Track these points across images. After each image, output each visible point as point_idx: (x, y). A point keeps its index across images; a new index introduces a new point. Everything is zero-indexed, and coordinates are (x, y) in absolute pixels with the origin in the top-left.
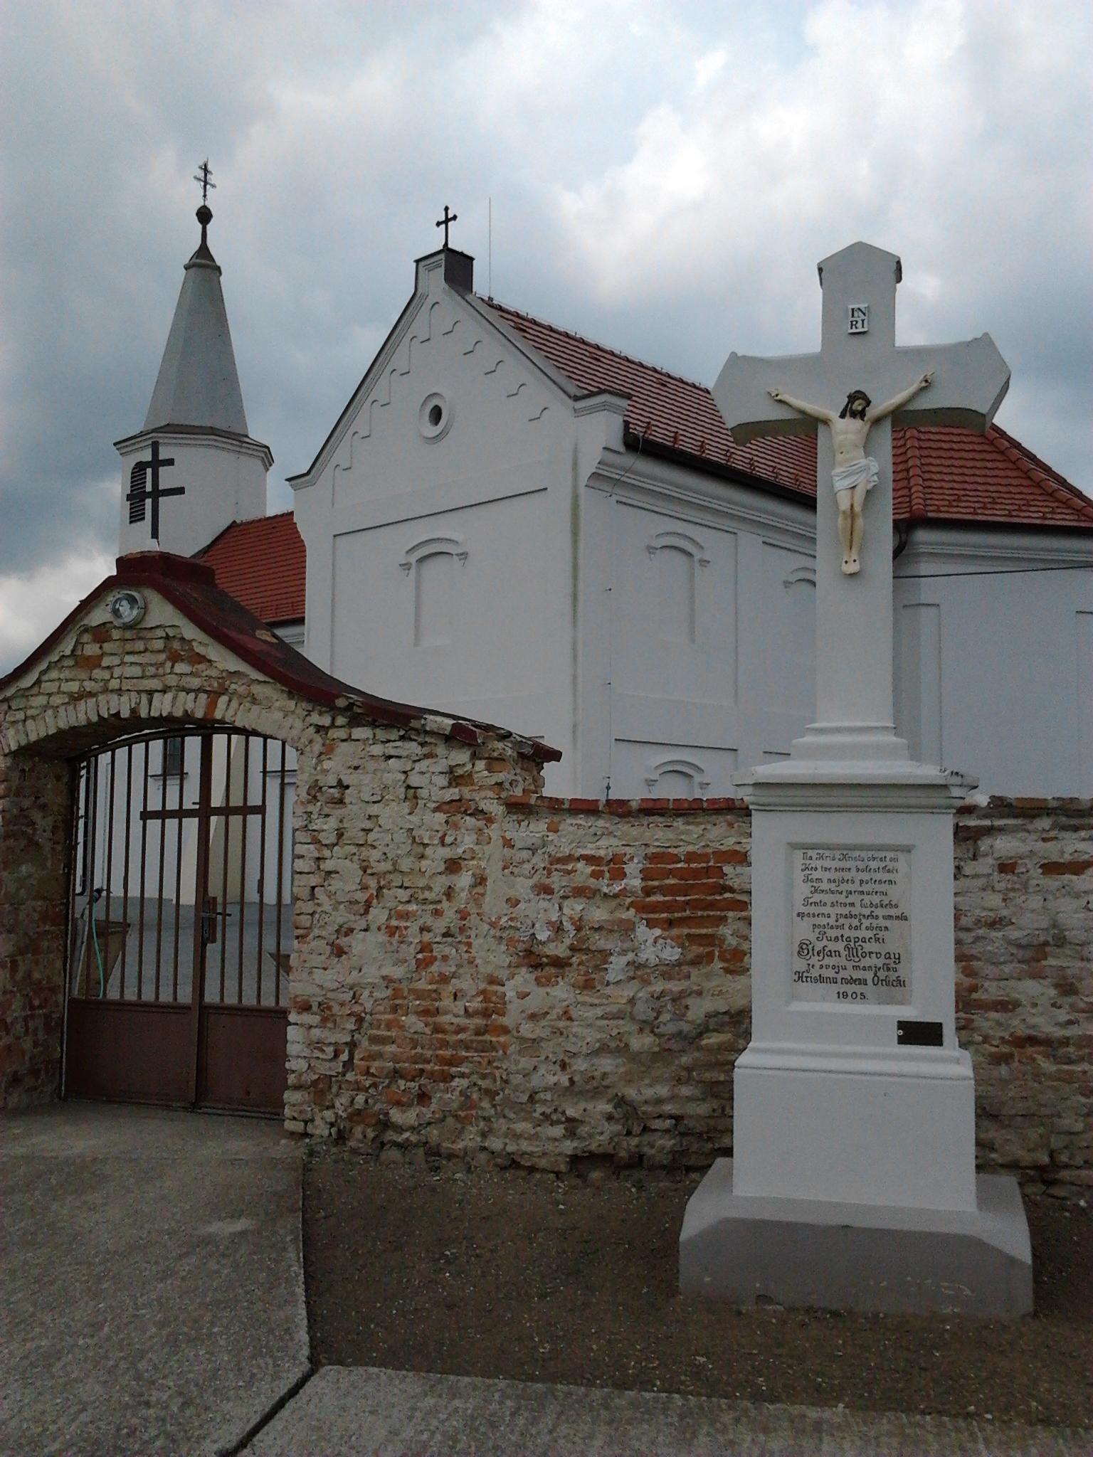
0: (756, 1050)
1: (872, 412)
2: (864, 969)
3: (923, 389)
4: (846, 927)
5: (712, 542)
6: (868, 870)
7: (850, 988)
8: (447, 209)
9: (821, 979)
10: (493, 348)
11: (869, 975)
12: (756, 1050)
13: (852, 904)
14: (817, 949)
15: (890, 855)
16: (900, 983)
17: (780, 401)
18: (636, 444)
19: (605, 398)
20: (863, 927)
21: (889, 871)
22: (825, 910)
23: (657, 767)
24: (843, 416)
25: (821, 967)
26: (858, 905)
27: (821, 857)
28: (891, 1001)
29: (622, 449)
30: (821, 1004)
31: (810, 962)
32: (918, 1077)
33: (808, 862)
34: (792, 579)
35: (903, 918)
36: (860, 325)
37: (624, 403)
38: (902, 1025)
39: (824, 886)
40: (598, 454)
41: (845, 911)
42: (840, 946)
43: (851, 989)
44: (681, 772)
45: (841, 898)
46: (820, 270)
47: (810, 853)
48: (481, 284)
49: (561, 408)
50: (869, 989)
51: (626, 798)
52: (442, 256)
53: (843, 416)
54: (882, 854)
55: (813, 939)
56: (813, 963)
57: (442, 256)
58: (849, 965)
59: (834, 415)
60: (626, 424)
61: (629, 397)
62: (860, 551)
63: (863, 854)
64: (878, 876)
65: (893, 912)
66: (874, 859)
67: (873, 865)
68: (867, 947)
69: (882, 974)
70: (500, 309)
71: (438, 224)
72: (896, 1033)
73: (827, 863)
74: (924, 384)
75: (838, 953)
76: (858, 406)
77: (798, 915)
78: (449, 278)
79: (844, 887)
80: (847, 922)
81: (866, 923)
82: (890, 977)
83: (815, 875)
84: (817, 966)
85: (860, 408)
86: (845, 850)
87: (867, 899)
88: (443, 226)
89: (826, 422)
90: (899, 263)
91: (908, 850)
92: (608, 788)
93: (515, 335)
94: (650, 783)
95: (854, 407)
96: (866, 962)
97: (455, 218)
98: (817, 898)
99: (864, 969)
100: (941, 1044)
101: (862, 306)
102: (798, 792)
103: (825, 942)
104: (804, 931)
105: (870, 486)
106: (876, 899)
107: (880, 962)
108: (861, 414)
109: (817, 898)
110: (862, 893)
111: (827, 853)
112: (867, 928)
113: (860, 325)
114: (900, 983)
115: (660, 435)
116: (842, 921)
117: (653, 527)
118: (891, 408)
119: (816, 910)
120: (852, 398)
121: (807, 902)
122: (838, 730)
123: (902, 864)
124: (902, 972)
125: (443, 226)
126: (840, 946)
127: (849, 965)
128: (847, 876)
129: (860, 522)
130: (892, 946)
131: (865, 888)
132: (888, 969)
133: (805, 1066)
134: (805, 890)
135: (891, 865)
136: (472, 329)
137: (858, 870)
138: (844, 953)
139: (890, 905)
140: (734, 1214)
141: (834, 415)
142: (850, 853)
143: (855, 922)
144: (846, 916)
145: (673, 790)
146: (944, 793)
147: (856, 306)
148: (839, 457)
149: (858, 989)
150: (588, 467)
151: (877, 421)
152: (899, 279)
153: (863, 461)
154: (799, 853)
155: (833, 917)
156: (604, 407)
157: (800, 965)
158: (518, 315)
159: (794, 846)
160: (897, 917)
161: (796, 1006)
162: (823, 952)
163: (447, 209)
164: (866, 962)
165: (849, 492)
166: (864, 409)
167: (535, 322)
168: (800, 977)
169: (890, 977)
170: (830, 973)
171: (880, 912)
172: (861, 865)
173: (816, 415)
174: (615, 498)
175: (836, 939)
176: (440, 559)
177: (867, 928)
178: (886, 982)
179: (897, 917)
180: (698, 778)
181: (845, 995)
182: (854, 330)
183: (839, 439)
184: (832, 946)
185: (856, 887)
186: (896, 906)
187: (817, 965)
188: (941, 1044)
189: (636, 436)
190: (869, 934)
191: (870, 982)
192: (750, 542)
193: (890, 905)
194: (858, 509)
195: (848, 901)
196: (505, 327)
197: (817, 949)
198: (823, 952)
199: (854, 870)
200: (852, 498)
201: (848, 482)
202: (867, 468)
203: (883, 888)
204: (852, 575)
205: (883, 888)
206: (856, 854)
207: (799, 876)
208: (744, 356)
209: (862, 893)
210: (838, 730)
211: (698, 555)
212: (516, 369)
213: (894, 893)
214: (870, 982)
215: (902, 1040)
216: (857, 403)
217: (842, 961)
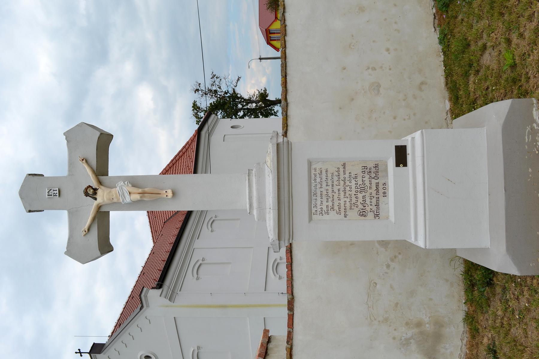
0: (416, 239)
1: (95, 184)
2: (370, 184)
3: (87, 161)
4: (350, 193)
5: (197, 257)
6: (321, 183)
7: (381, 191)
8: (76, 353)
9: (377, 205)
10: (125, 337)
11: (374, 182)
12: (416, 239)
13: (339, 190)
14: (362, 207)
15: (313, 172)
16: (376, 166)
17: (89, 230)
18: (160, 286)
19: (142, 295)
20: (350, 184)
21: (321, 172)
22: (342, 205)
23: (275, 275)
24: (96, 199)
25: (371, 205)
26: (339, 187)
27: (316, 206)
28: (386, 170)
29: (161, 290)
30: (390, 204)
31: (369, 210)
32: (423, 156)
33: (318, 212)
34: (210, 229)
35: (344, 165)
36: (55, 192)
37: (145, 289)
38: (398, 165)
39: (330, 204)
40: (162, 298)
41: (342, 194)
42: (360, 196)
43: (381, 191)
44: (276, 266)
45: (336, 196)
46: (30, 211)
47: (313, 211)
48: (104, 340)
49: (147, 312)
50: (381, 181)
51: (287, 316)
52: (92, 355)
53: (96, 199)
54: (313, 176)
55: (357, 209)
56: (371, 209)
57: (92, 355)
58: (369, 191)
59: (95, 203)
60: (153, 288)
61: (143, 287)
62: (162, 189)
63: (313, 185)
64: (324, 178)
65: (342, 170)
66: (315, 180)
67: (318, 180)
68: (360, 182)
69: (373, 175)
70: (113, 333)
71: (81, 356)
72: (401, 168)
73: (319, 203)
74: (84, 161)
75: (364, 197)
76: (91, 192)
77: (345, 217)
78: (99, 353)
79: (330, 194)
80: (348, 193)
81: (348, 183)
82: (375, 171)
83: (325, 208)
84: (371, 207)
85: (92, 190)
86: (311, 194)
87: (336, 183)
88: (82, 354)
89: (99, 207)
90: (29, 175)
91: (310, 163)
92: (282, 293)
93: (122, 326)
94: (280, 278)
95: (91, 193)
96: (367, 183)
97: (79, 350)
98: (336, 208)
99: (370, 184)
100: (405, 146)
101: (47, 191)
102: (282, 182)
103: (359, 203)
104: (353, 214)
105: (130, 185)
106: (336, 178)
107: (367, 176)
108: (95, 190)
109: (336, 208)
110: (333, 185)
111: (313, 203)
112: (350, 182)
113: (55, 192)
114: (376, 166)
115: (158, 275)
116: (347, 195)
117: (190, 279)
118: (94, 176)
119: (343, 208)
120: (87, 194)
121: (339, 213)
122: (250, 198)
123: (318, 166)
124: (371, 165)
125: (82, 354)
126: (360, 196)
127: (369, 191)
128: (324, 193)
129: (146, 190)
130: (358, 170)
131: (330, 183)
132: (370, 172)
133: (422, 212)
134: (332, 214)
135: (318, 171)
136: (118, 345)
137: (321, 188)
138: (364, 194)
139: (338, 171)
140: (503, 247)
141: (95, 203)
142: (313, 191)
143: (348, 188)
144: (345, 193)
145: (283, 270)
146: (281, 146)
147: (47, 194)
148: (115, 200)
149: (381, 187)
150: (167, 301)
151: (100, 183)
152: (42, 175)
153: (118, 188)
154: (314, 217)
155: (346, 199)
156: (146, 296)
157: (371, 215)
158: (116, 326)
159: (310, 219)
160: (344, 168)
161: (392, 219)
162: (364, 204)
163: (76, 353)
164: (367, 183)
165: (132, 195)
166: (93, 189)
167: (119, 320)
168: (377, 216)
169: (375, 171)
170: (374, 200)
171: (342, 177)
172: (319, 186)
173: (95, 212)
174: (178, 292)
175: (356, 198)
176: (200, 354)
177: (350, 182)
178: (377, 172)
179: (344, 168)
180: (278, 261)
181: (384, 193)
182: (58, 194)
183: (106, 201)
184: (360, 200)
185: (330, 188)
186: (338, 168)
187: (370, 207)
188: (405, 146)
189: (158, 285)
190: (353, 182)
191: (377, 181)
192: (197, 244)
193: (338, 171)
194: (140, 190)
195: (337, 192)
196: (119, 330)
197: (362, 207)
198: (364, 204)
199: (322, 190)
200: (134, 193)
201: (127, 195)
202: (121, 188)
203: (330, 175)
204: (174, 193)
205: (330, 175)
206: (313, 188)
207: (325, 217)
208: (67, 248)
209: (333, 185)
210: (250, 198)
211: (200, 262)
212: (133, 329)
213: (332, 170)
214: (377, 181)
215: (405, 165)
216: (89, 192)
217: (368, 195)
